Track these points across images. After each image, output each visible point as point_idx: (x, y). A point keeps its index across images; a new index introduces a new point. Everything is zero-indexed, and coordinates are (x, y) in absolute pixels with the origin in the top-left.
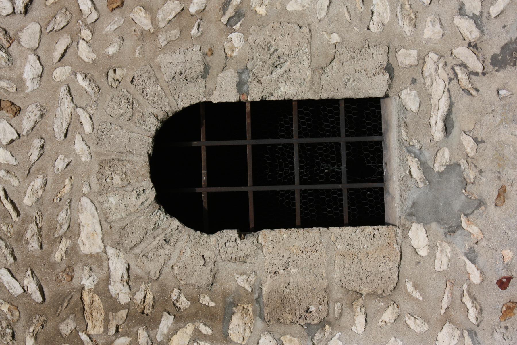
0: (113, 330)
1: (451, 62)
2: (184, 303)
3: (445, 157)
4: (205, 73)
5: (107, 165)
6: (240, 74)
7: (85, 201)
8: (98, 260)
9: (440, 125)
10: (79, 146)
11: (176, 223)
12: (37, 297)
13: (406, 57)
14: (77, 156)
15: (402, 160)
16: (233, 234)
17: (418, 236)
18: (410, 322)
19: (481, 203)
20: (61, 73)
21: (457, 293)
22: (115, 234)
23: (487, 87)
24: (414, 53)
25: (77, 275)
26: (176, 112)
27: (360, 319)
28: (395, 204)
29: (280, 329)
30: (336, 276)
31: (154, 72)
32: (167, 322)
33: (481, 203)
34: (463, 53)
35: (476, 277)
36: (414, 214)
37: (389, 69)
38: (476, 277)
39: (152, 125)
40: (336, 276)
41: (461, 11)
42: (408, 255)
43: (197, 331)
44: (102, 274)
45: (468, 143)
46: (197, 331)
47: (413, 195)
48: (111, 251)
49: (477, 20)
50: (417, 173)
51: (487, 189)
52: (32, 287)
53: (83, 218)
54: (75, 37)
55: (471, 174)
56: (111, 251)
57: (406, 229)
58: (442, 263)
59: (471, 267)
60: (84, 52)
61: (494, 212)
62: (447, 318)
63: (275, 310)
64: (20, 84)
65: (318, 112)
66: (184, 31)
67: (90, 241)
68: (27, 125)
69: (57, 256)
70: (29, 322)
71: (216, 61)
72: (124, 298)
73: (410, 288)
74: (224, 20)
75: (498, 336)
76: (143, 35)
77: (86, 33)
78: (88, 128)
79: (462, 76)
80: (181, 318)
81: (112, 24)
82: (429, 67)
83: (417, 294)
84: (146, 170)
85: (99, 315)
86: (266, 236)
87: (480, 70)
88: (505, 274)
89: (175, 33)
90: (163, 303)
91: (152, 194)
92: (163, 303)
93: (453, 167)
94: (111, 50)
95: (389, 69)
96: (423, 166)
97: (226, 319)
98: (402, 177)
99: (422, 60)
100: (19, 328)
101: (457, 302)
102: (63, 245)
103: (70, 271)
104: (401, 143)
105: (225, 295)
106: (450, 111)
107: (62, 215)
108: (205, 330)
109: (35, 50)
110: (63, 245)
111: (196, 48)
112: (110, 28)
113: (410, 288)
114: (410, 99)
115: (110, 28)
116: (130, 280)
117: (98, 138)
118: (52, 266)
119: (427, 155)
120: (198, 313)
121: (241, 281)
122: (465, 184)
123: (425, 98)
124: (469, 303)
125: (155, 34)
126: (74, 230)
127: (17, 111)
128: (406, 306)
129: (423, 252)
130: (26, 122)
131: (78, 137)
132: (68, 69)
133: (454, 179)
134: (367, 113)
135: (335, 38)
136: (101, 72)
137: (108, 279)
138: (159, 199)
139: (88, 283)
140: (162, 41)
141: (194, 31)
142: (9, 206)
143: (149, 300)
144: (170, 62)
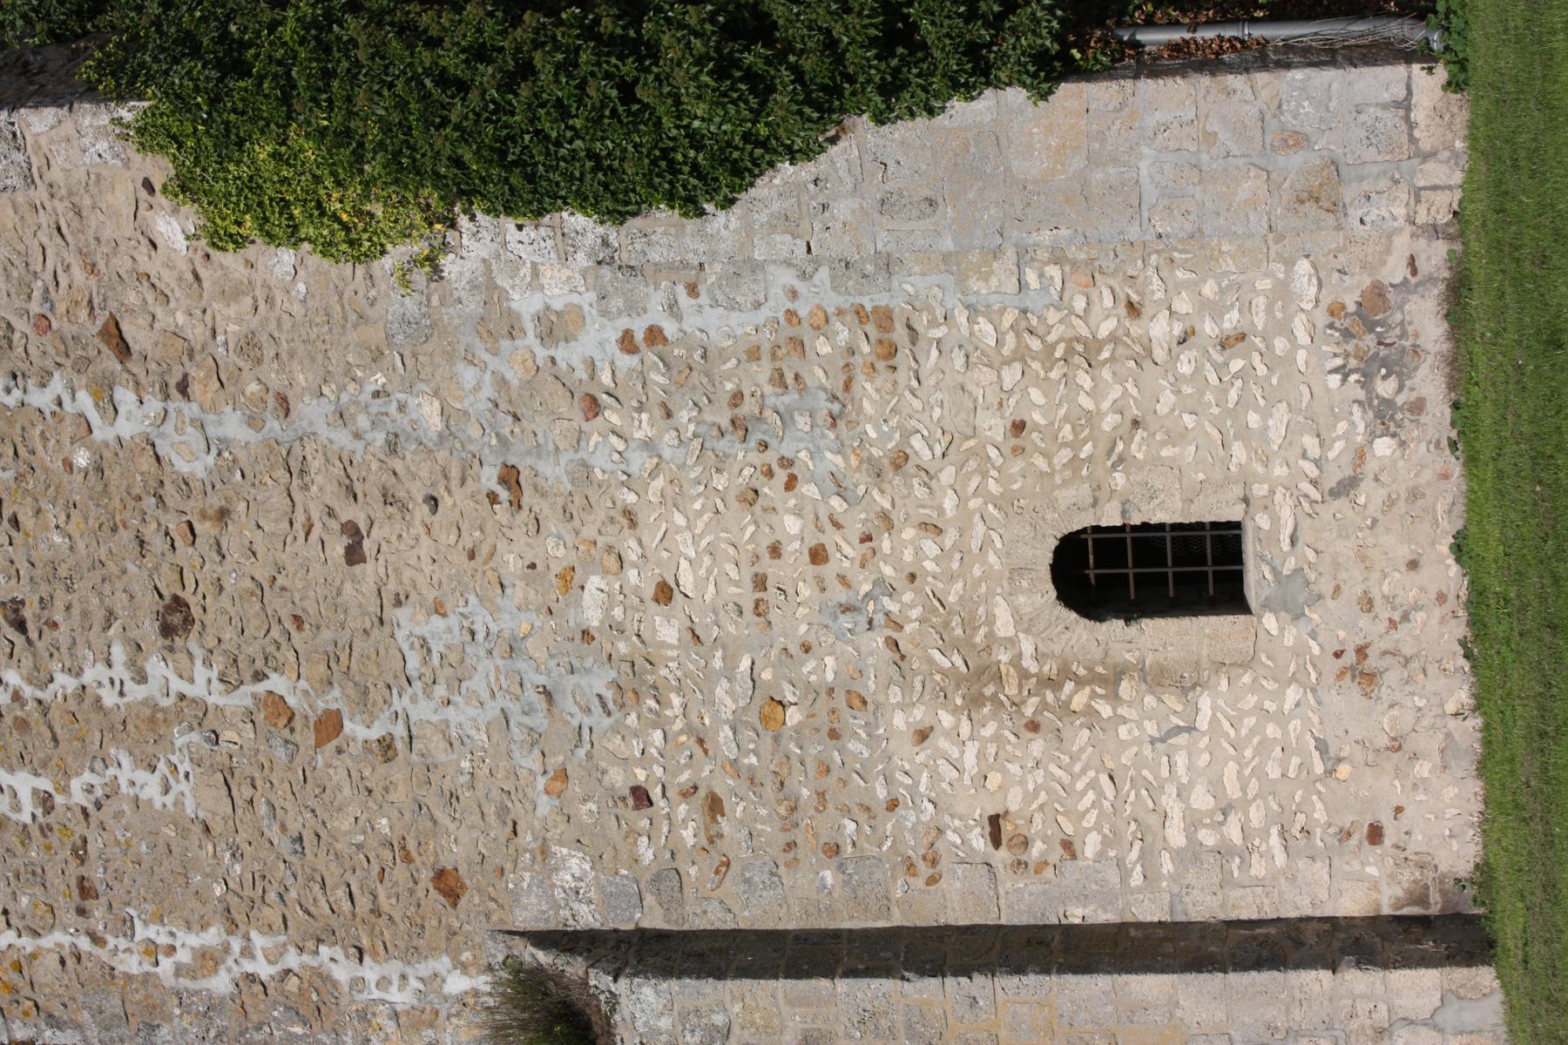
0: (1026, 693)
1: (1296, 493)
2: (1082, 672)
3: (1291, 564)
4: (1095, 504)
5: (1017, 572)
6: (1123, 504)
7: (999, 599)
8: (1011, 642)
9: (1288, 540)
11: (1074, 615)
12: (964, 669)
13: (1259, 490)
14: (991, 566)
15: (1257, 567)
16: (1121, 622)
17: (1270, 622)
18: (1264, 683)
19: (1320, 597)
20: (974, 504)
21: (1301, 661)
22: (1025, 623)
23: (1326, 512)
24: (1266, 487)
25: (994, 652)
27: (1224, 682)
28: (1253, 602)
29: (1160, 689)
30: (1204, 652)
31: (1052, 504)
32: (1069, 686)
33: (1320, 597)
34: (1306, 487)
35: (1316, 650)
36: (1266, 606)
37: (1246, 500)
38: (1316, 650)
39: (1053, 543)
40: (1204, 652)
41: (1304, 456)
42: (1261, 634)
43: (1093, 691)
44: (1016, 651)
46: (1093, 691)
47: (1266, 592)
48: (1021, 635)
50: (1268, 576)
51: (1326, 587)
52: (959, 662)
53: (997, 611)
55: (1312, 576)
56: (1021, 635)
57: (1260, 617)
58: (1289, 640)
59: (1312, 643)
60: (993, 487)
61: (1330, 604)
62: (1293, 679)
63: (1156, 678)
64: (941, 511)
65: (1237, 579)
67: (1004, 626)
68: (948, 543)
69: (978, 639)
70: (958, 686)
72: (1034, 668)
73: (1264, 659)
74: (1109, 463)
75: (1334, 692)
76: (1042, 474)
77: (994, 473)
78: (999, 545)
79: (1305, 505)
80: (1080, 683)
81: (1017, 466)
82: (1278, 497)
83: (1269, 663)
84: (1048, 577)
85: (1014, 681)
86: (1148, 624)
87: (1319, 498)
88: (1338, 648)
89: (1068, 473)
90: (1066, 673)
91: (1054, 594)
92: (1066, 673)
93: (1298, 571)
94: (1015, 487)
95: (1246, 500)
96: (1274, 570)
97: (1117, 683)
98: (1257, 579)
99: (1272, 492)
100: (949, 691)
102: (982, 631)
104: (1256, 555)
105: (1115, 666)
106: (1295, 529)
107: (981, 610)
108: (1100, 691)
109: (952, 487)
110: (982, 631)
111: (1087, 485)
112: (1015, 470)
113: (1264, 659)
114: (1263, 521)
115: (1015, 470)
116: (1038, 657)
118: (974, 646)
119: (1277, 562)
120: (1094, 679)
121: (1128, 656)
122: (1307, 583)
123: (1275, 520)
124: (1310, 669)
125: (1051, 475)
126: (990, 620)
127: (939, 531)
128: (1262, 671)
129: (1275, 633)
131: (991, 552)
132: (980, 500)
133: (1299, 580)
135: (1201, 476)
137: (1020, 655)
138: (1059, 598)
139: (1004, 657)
140: (1058, 480)
141: (1084, 472)
142: (937, 604)
143: (1055, 671)
144: (1065, 496)
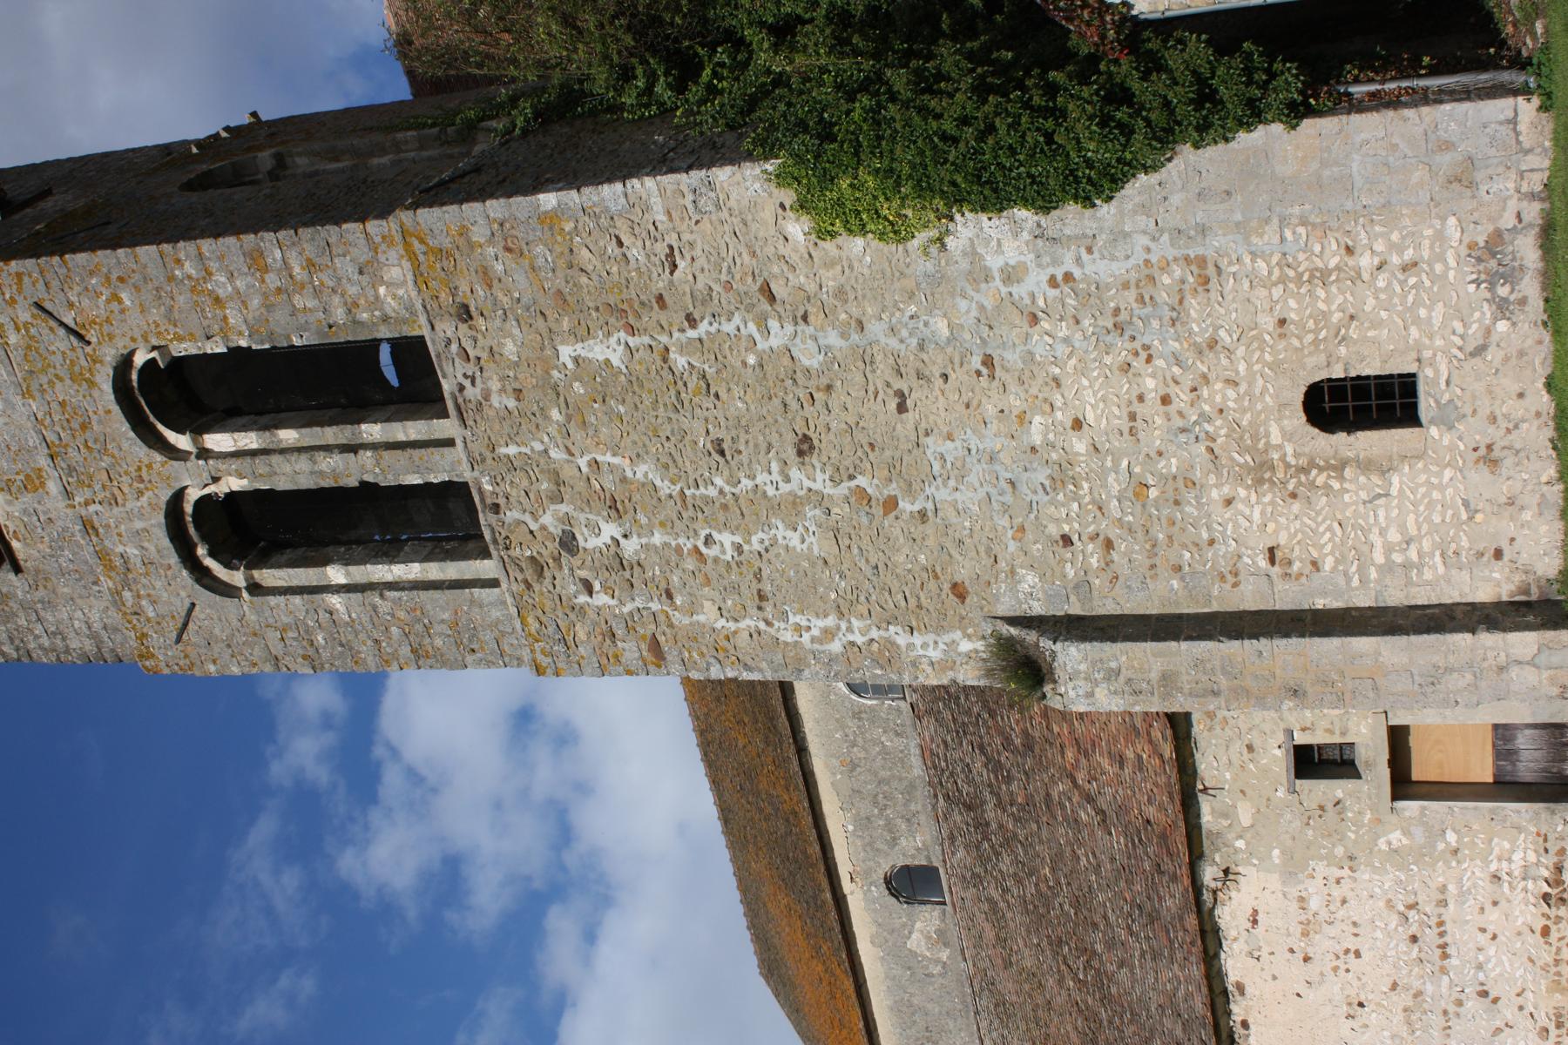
2: (1322, 463)
3: (1447, 397)
5: (1282, 406)
8: (1280, 447)
10: (1268, 399)
13: (1427, 354)
17: (1434, 431)
19: (1464, 416)
20: (1256, 367)
22: (1287, 436)
23: (1467, 366)
26: (1349, 433)
32: (1314, 472)
33: (1464, 416)
34: (1455, 351)
35: (1462, 447)
36: (1432, 422)
37: (1419, 360)
38: (1462, 447)
39: (1304, 389)
41: (1454, 333)
45: (1458, 391)
47: (1431, 414)
49: (1462, 337)
51: (1468, 410)
52: (1249, 459)
54: (1263, 351)
58: (1446, 442)
60: (1268, 357)
61: (1470, 419)
62: (1449, 464)
63: (1366, 466)
64: (1237, 373)
66: (1317, 347)
67: (1276, 438)
71: (1333, 359)
81: (1281, 345)
82: (1438, 358)
86: (1360, 434)
90: (1312, 464)
92: (1312, 464)
93: (1451, 401)
95: (1419, 360)
96: (1437, 402)
97: (1343, 469)
101: (1453, 458)
103: (1266, 451)
114: (1429, 372)
116: (1296, 455)
117: (1276, 396)
123: (1437, 371)
125: (1302, 349)
126: (1267, 435)
127: (1236, 384)
130: (1243, 388)
134: (1412, 377)
136: (1275, 366)
139: (1276, 456)
144: (1311, 361)
